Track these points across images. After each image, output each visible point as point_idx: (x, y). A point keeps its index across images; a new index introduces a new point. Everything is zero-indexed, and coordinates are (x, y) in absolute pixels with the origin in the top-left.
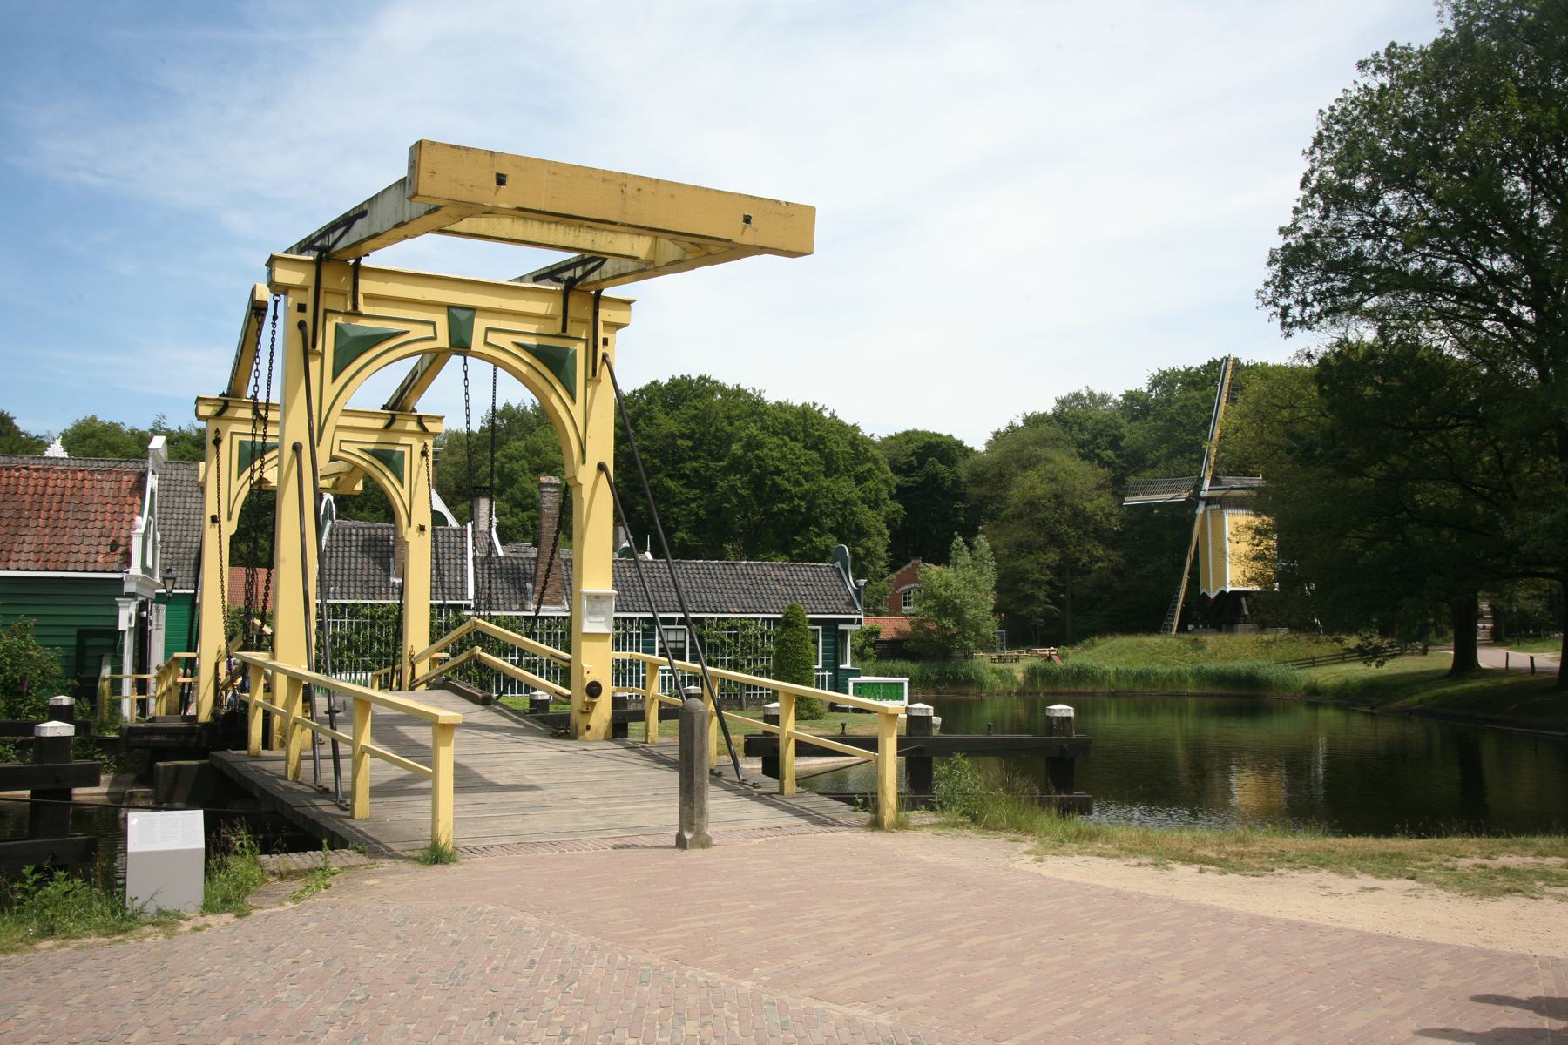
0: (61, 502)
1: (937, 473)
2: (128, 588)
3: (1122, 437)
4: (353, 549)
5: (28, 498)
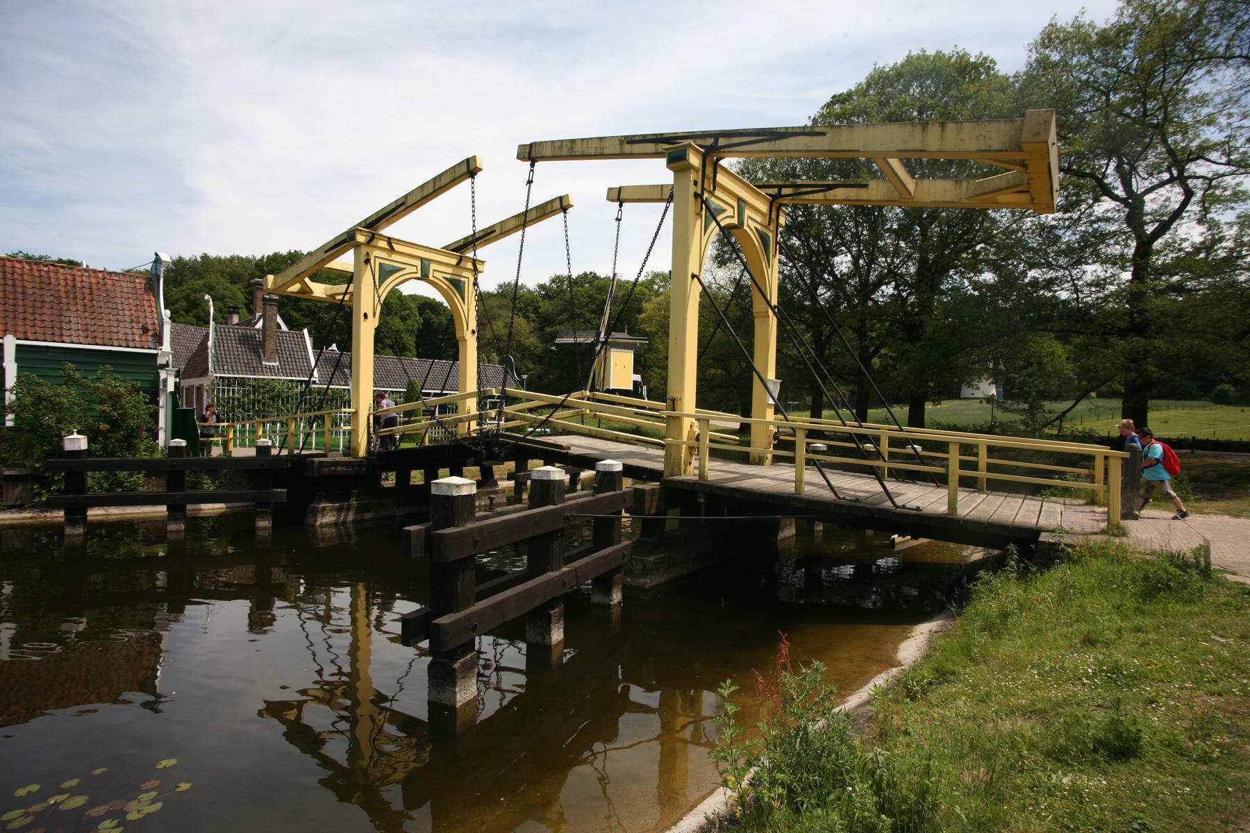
2: (161, 361)
3: (540, 307)
4: (234, 342)
5: (63, 289)
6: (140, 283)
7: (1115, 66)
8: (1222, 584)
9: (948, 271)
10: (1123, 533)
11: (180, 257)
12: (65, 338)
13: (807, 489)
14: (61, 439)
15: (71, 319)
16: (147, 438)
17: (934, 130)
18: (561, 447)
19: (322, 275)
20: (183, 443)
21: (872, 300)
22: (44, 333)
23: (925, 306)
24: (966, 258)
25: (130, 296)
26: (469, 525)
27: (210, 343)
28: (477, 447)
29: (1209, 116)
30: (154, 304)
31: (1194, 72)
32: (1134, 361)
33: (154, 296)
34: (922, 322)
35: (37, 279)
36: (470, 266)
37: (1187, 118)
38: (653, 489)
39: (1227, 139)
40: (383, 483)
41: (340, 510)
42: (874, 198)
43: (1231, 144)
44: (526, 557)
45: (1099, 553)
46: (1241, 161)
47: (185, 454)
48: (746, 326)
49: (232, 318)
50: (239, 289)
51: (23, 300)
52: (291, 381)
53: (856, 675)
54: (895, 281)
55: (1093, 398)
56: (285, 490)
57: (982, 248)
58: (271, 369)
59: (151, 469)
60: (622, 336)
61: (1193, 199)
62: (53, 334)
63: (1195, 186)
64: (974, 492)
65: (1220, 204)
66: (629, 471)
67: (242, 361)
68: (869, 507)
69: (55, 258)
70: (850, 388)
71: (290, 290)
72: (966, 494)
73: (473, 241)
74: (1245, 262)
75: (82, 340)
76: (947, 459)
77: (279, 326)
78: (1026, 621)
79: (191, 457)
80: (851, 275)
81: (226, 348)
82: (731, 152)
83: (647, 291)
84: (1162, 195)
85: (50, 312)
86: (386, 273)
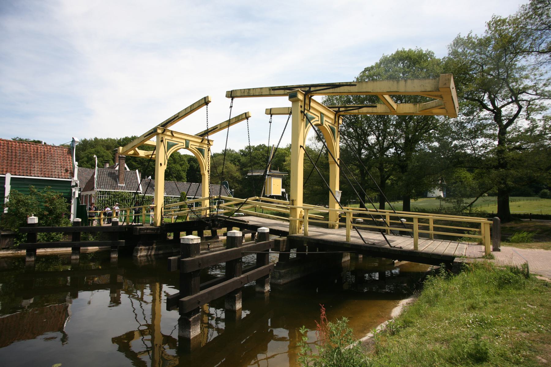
0: (45, 155)
1: (193, 165)
2: (73, 184)
3: (241, 160)
5: (32, 153)
6: (66, 150)
7: (485, 54)
8: (535, 280)
9: (418, 142)
10: (492, 257)
11: (85, 139)
12: (32, 174)
13: (352, 240)
14: (27, 218)
15: (35, 166)
16: (65, 218)
17: (402, 83)
18: (245, 221)
19: (142, 147)
20: (80, 220)
21: (386, 155)
22: (23, 172)
23: (408, 157)
24: (426, 136)
25: (61, 156)
26: (197, 257)
27: (95, 176)
28: (208, 221)
29: (526, 75)
30: (71, 160)
31: (518, 57)
32: (502, 179)
33: (71, 156)
34: (407, 164)
35: (22, 149)
36: (206, 142)
37: (517, 76)
38: (284, 240)
39: (535, 85)
40: (168, 237)
41: (148, 250)
42: (379, 112)
43: (537, 87)
44: (69, 277)
45: (480, 267)
46: (542, 93)
47: (81, 225)
48: (326, 167)
49: (106, 165)
50: (110, 152)
51: (15, 158)
52: (130, 192)
53: (372, 323)
54: (395, 146)
55: (486, 196)
56: (124, 241)
57: (433, 132)
58: (122, 187)
59: (66, 231)
60: (277, 172)
61: (523, 110)
62: (27, 173)
63: (523, 105)
64: (428, 239)
65: (535, 111)
66: (273, 232)
67: (109, 184)
68: (379, 247)
69: (32, 140)
70: (378, 193)
71: (129, 153)
72: (424, 240)
73: (207, 132)
74: (548, 136)
75: (39, 175)
76: (413, 225)
77: (126, 169)
78: (447, 299)
79: (84, 226)
80: (375, 144)
81: (102, 178)
82: (316, 93)
83: (287, 152)
84: (509, 108)
85: (26, 163)
86: (170, 146)
